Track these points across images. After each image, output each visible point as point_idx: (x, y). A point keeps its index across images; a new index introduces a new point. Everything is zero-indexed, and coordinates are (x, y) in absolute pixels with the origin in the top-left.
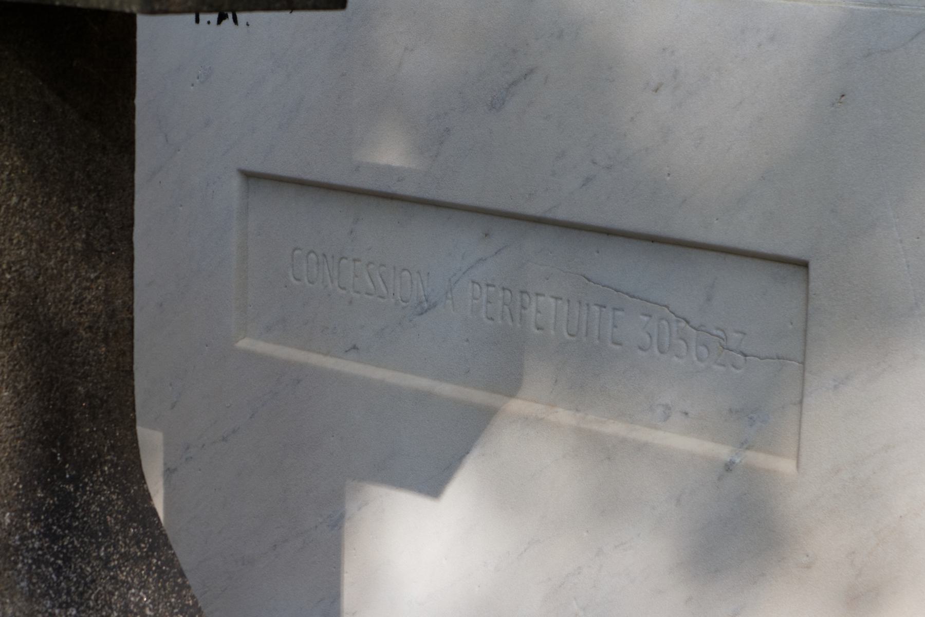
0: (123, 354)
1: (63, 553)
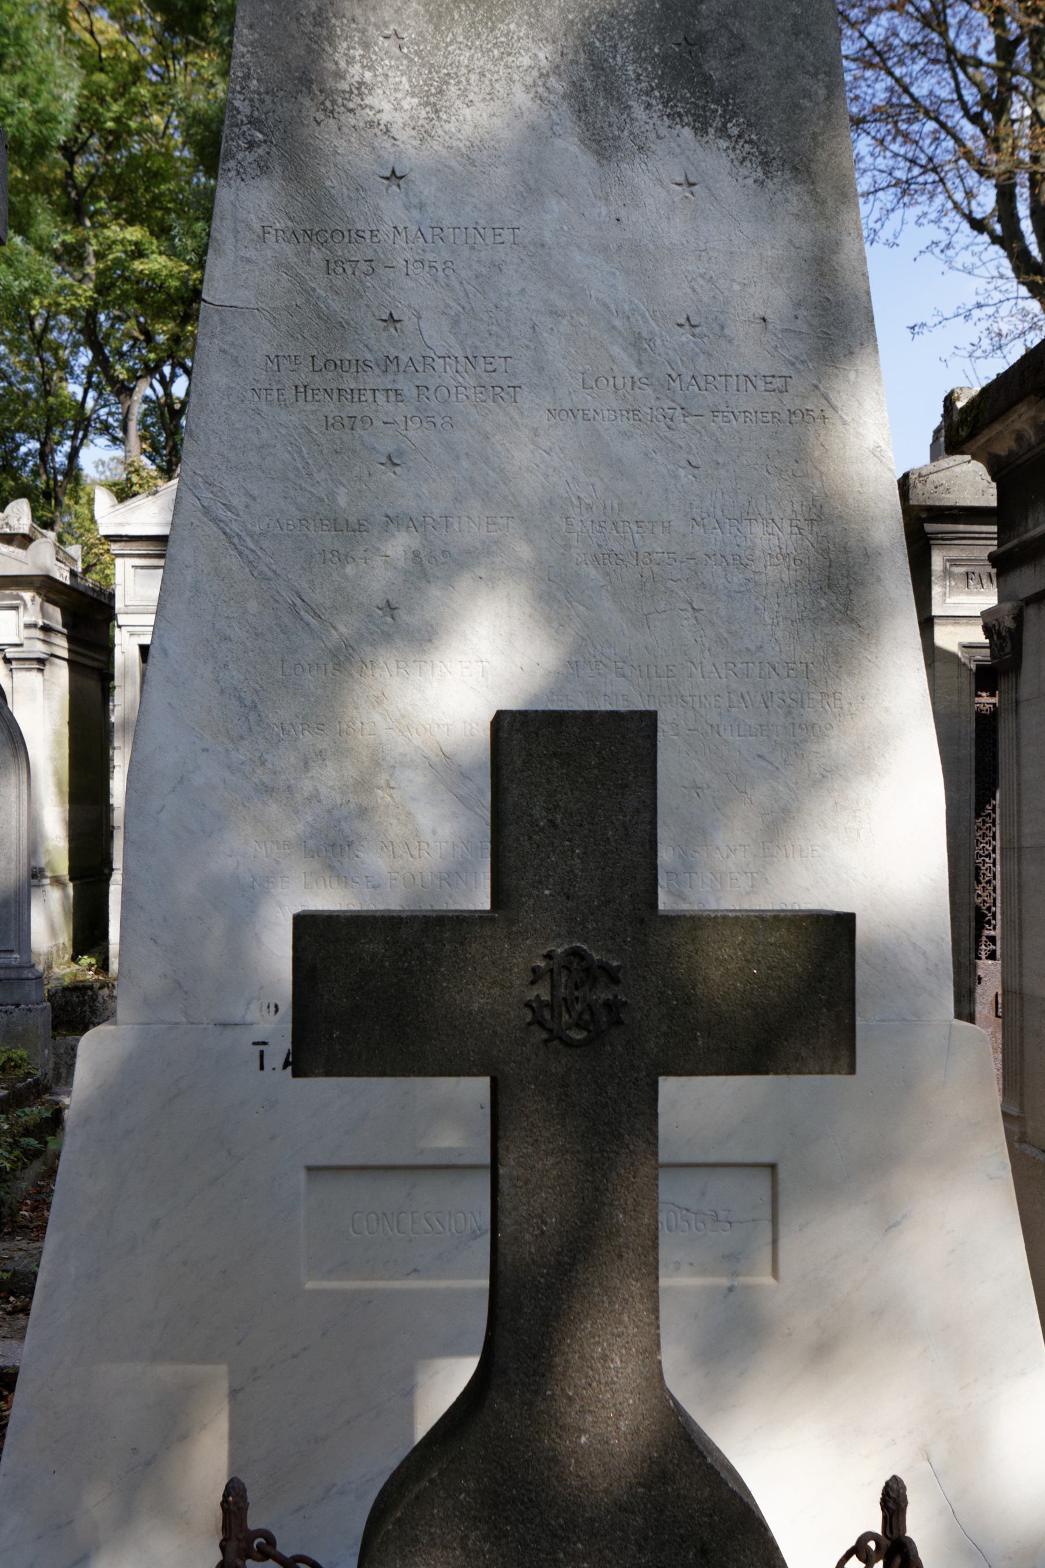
0: (1023, 1139)
1: (512, 1542)
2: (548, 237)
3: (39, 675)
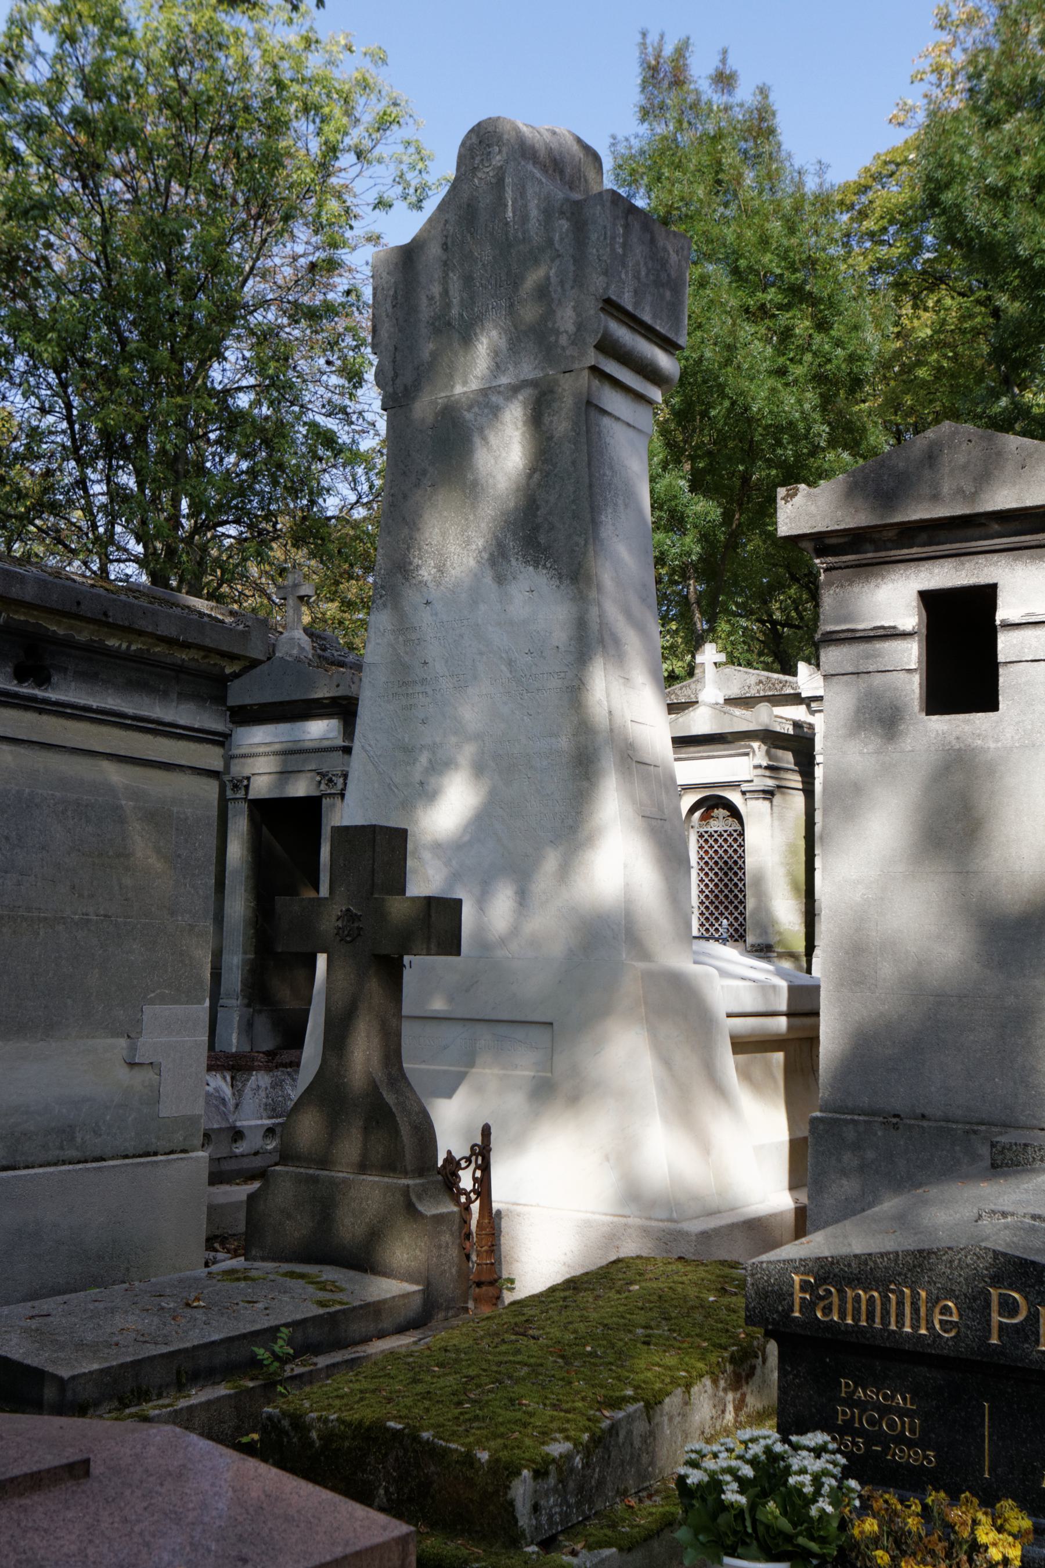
2: (480, 621)
3: (767, 803)
